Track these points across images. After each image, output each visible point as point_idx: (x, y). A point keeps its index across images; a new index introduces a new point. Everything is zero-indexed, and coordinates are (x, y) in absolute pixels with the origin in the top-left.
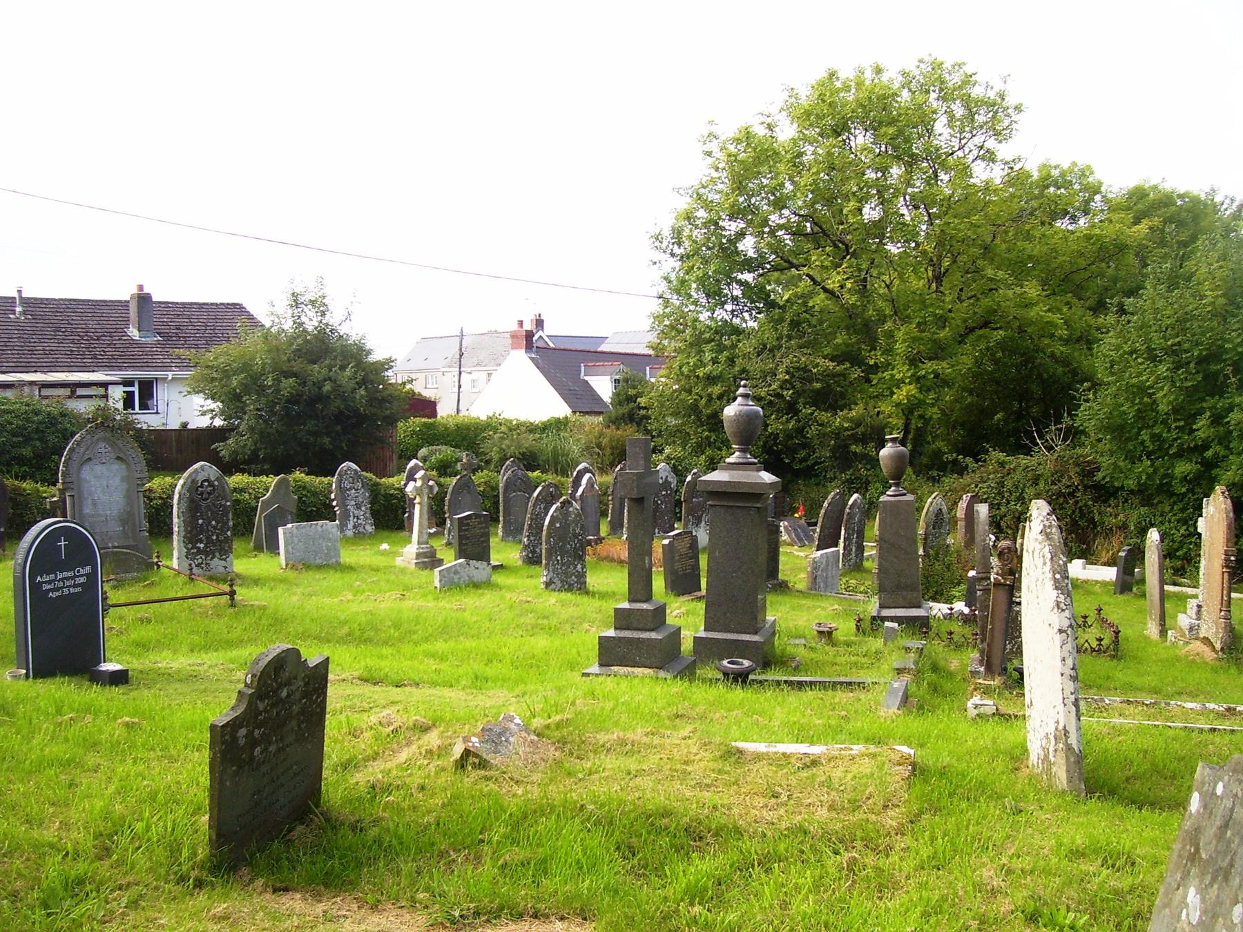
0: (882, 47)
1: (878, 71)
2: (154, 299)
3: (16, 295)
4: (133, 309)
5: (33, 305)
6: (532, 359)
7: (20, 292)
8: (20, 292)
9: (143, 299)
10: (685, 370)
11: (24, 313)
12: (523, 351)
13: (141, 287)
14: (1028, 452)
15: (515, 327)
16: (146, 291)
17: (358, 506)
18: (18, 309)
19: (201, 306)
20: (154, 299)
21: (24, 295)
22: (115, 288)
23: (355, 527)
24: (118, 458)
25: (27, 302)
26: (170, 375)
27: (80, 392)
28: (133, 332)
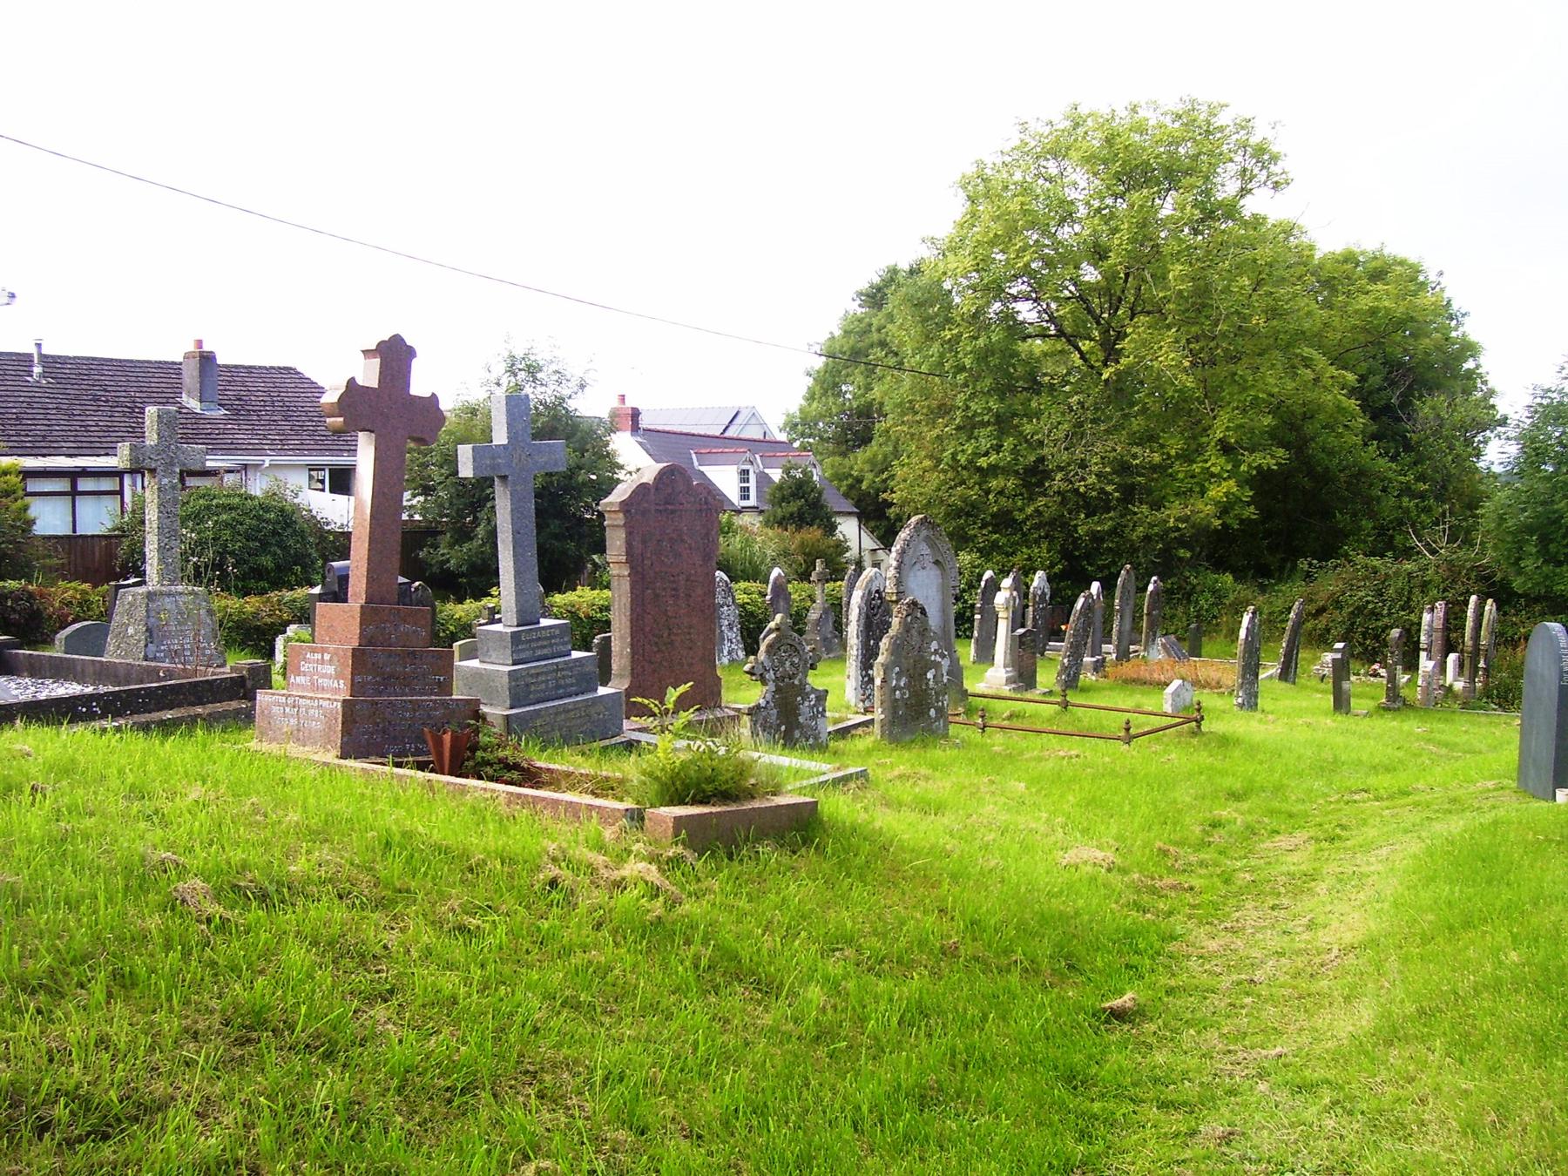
0: (1140, 83)
1: (1134, 110)
2: (219, 362)
3: (33, 350)
4: (190, 376)
5: (53, 364)
6: (640, 444)
7: (39, 346)
8: (39, 346)
9: (206, 360)
10: (962, 459)
11: (43, 375)
12: (628, 433)
13: (199, 343)
14: (1408, 553)
15: (616, 404)
16: (206, 348)
17: (730, 627)
18: (37, 370)
19: (121, 364)
20: (219, 362)
21: (44, 352)
22: (159, 341)
23: (729, 653)
24: (937, 563)
25: (47, 360)
26: (267, 461)
27: (85, 485)
28: (194, 404)
